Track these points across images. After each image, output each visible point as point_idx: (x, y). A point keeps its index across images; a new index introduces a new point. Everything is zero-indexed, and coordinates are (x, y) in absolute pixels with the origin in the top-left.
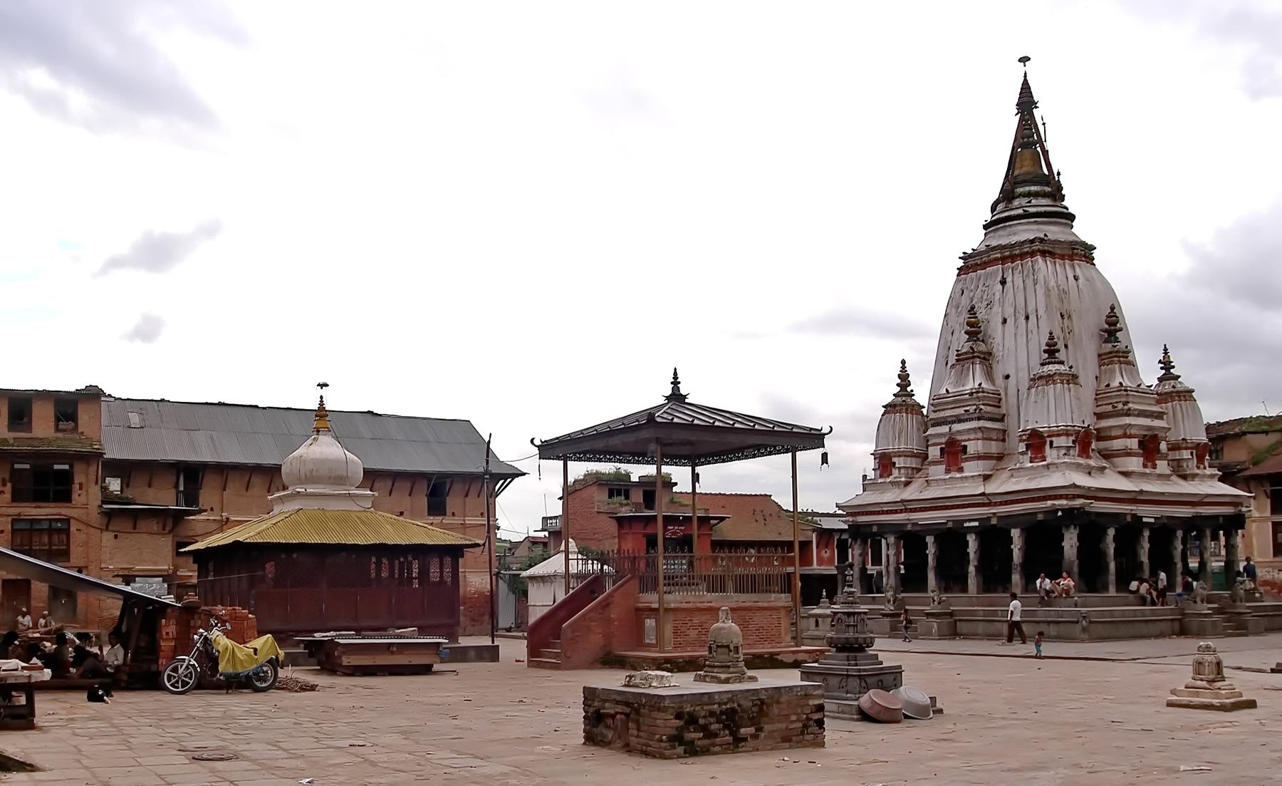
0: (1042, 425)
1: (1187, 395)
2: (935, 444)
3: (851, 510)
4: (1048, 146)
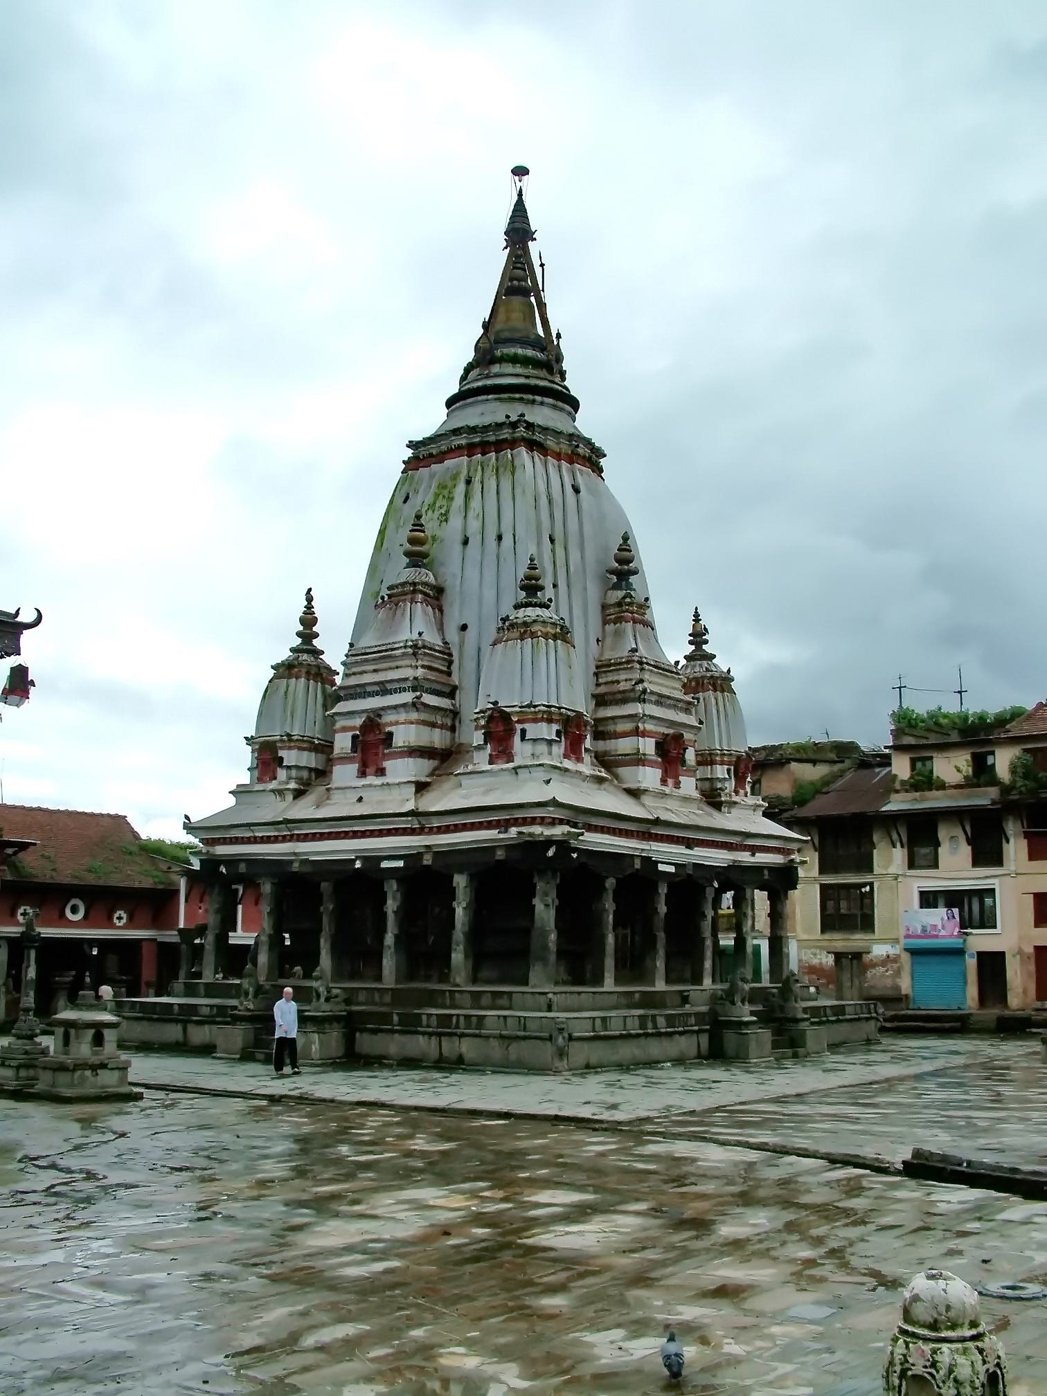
0: (510, 701)
1: (722, 683)
2: (344, 729)
3: (210, 832)
4: (548, 297)
